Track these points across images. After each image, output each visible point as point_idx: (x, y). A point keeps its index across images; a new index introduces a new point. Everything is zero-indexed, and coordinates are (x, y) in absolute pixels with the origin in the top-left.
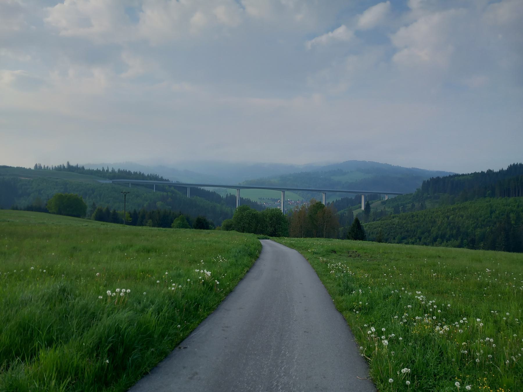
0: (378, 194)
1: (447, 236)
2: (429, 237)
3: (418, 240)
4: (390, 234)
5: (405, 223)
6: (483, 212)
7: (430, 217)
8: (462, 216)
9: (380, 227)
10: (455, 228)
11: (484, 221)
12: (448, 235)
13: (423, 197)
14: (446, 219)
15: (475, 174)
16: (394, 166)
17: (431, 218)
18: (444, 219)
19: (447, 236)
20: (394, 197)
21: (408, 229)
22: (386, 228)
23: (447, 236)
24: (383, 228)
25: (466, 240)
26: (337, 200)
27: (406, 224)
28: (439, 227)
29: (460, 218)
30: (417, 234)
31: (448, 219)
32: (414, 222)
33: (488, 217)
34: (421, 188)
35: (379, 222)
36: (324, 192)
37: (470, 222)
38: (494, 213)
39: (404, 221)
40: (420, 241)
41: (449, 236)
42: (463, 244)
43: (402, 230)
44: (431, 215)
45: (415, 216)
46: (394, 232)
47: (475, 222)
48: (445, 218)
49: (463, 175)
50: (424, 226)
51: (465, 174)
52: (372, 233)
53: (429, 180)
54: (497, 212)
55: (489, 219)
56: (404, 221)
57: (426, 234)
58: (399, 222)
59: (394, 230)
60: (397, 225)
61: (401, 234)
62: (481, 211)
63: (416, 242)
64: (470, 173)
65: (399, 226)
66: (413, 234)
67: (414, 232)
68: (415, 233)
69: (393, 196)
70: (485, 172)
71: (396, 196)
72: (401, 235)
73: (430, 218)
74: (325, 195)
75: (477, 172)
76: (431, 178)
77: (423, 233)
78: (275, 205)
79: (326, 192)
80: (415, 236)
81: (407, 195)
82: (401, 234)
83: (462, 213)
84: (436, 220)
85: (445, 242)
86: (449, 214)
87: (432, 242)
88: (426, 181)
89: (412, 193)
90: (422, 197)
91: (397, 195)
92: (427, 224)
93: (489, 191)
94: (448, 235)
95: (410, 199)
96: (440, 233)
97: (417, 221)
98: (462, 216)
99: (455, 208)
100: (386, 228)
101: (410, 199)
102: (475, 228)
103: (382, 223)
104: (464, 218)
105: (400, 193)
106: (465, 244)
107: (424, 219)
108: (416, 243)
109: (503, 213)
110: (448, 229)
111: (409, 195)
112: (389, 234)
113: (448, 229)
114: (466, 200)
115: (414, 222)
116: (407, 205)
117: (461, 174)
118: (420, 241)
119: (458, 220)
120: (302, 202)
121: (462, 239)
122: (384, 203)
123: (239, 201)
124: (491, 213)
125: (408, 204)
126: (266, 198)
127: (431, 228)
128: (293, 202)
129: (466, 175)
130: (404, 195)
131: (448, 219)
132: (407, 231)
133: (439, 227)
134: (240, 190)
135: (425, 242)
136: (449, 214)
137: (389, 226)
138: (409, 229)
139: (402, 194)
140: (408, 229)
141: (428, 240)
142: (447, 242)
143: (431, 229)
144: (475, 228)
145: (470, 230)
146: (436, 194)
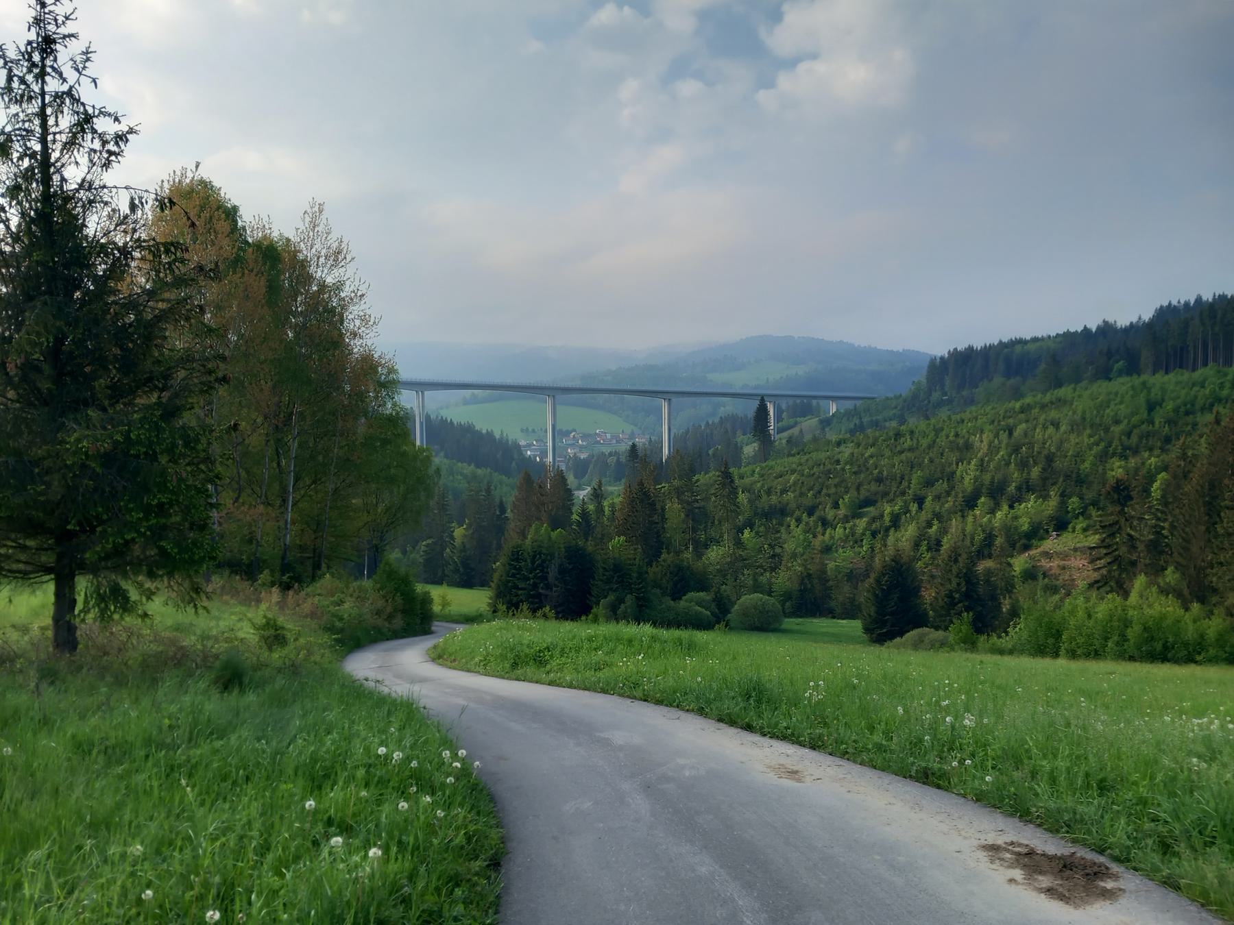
0: (814, 402)
1: (1009, 489)
2: (948, 494)
3: (914, 507)
4: (824, 491)
5: (871, 456)
6: (1122, 407)
7: (952, 434)
8: (1056, 425)
9: (793, 472)
10: (1034, 461)
11: (1129, 435)
12: (1014, 484)
13: (929, 402)
14: (1004, 436)
15: (1068, 337)
16: (859, 346)
17: (957, 435)
18: (997, 436)
19: (1012, 488)
20: (852, 407)
21: (881, 472)
22: (812, 472)
23: (1012, 488)
24: (803, 475)
25: (1075, 499)
26: (708, 423)
27: (875, 458)
28: (982, 460)
29: (1051, 430)
30: (909, 488)
31: (1011, 434)
32: (903, 452)
33: (1143, 423)
34: (924, 381)
35: (795, 459)
36: (666, 396)
37: (1086, 440)
38: (1158, 408)
39: (871, 451)
40: (920, 508)
41: (1019, 488)
42: (1068, 512)
43: (862, 476)
44: (955, 427)
45: (904, 436)
46: (836, 486)
47: (1101, 440)
48: (1002, 432)
49: (1035, 340)
50: (931, 461)
51: (1040, 336)
52: (769, 492)
53: (947, 356)
54: (1170, 406)
55: (1144, 427)
56: (871, 451)
57: (941, 486)
58: (852, 454)
59: (837, 480)
60: (846, 463)
61: (858, 489)
62: (1116, 405)
63: (909, 511)
64: (1053, 334)
65: (851, 464)
66: (898, 487)
67: (901, 483)
68: (905, 484)
69: (849, 405)
70: (1094, 330)
71: (859, 403)
72: (859, 494)
73: (951, 438)
74: (669, 405)
75: (1072, 330)
76: (952, 350)
77: (929, 483)
78: (562, 445)
79: (669, 396)
80: (903, 493)
81: (887, 398)
82: (858, 489)
83: (1054, 414)
84: (970, 440)
85: (1005, 507)
86: (1011, 421)
87: (961, 511)
88: (938, 360)
89: (901, 395)
90: (926, 402)
91: (861, 402)
92: (942, 454)
93: (1121, 363)
94: (1014, 484)
95: (896, 408)
96: (987, 478)
97: (911, 449)
98: (1056, 425)
99: (1028, 405)
100: (814, 474)
101: (896, 408)
102: (1104, 457)
103: (803, 461)
104: (1063, 428)
105: (869, 395)
106: (1074, 510)
107: (934, 442)
108: (908, 515)
109: (1189, 406)
110: (1013, 465)
111: (892, 399)
112: (820, 492)
113: (1013, 465)
114: (1059, 384)
115: (901, 452)
116: (887, 424)
117: (1028, 338)
118: (920, 508)
119: (1044, 435)
120: (632, 436)
121: (1063, 495)
122: (826, 423)
123: (421, 423)
124: (1151, 407)
125: (891, 420)
126: (541, 429)
127: (957, 465)
128: (609, 436)
129: (1043, 339)
130: (878, 400)
131: (1011, 434)
132: (879, 480)
133: (982, 460)
134: (426, 393)
135: (937, 509)
136: (1011, 421)
137: (822, 467)
138: (885, 473)
139: (874, 398)
140: (881, 472)
141: (946, 505)
142: (1011, 507)
143: (957, 468)
144: (1104, 457)
145: (1087, 465)
146: (964, 393)
